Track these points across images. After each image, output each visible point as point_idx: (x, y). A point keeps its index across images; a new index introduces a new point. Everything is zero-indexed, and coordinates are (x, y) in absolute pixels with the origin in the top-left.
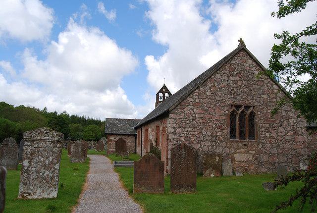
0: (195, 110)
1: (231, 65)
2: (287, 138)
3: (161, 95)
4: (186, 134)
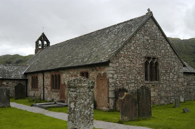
0: (125, 60)
2: (174, 80)
3: (40, 42)
4: (120, 78)
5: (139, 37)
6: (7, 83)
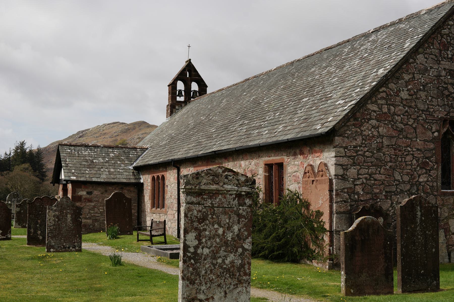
0: (381, 129)
1: (442, 37)
3: (180, 86)
4: (366, 178)
5: (424, 63)
6: (88, 193)
